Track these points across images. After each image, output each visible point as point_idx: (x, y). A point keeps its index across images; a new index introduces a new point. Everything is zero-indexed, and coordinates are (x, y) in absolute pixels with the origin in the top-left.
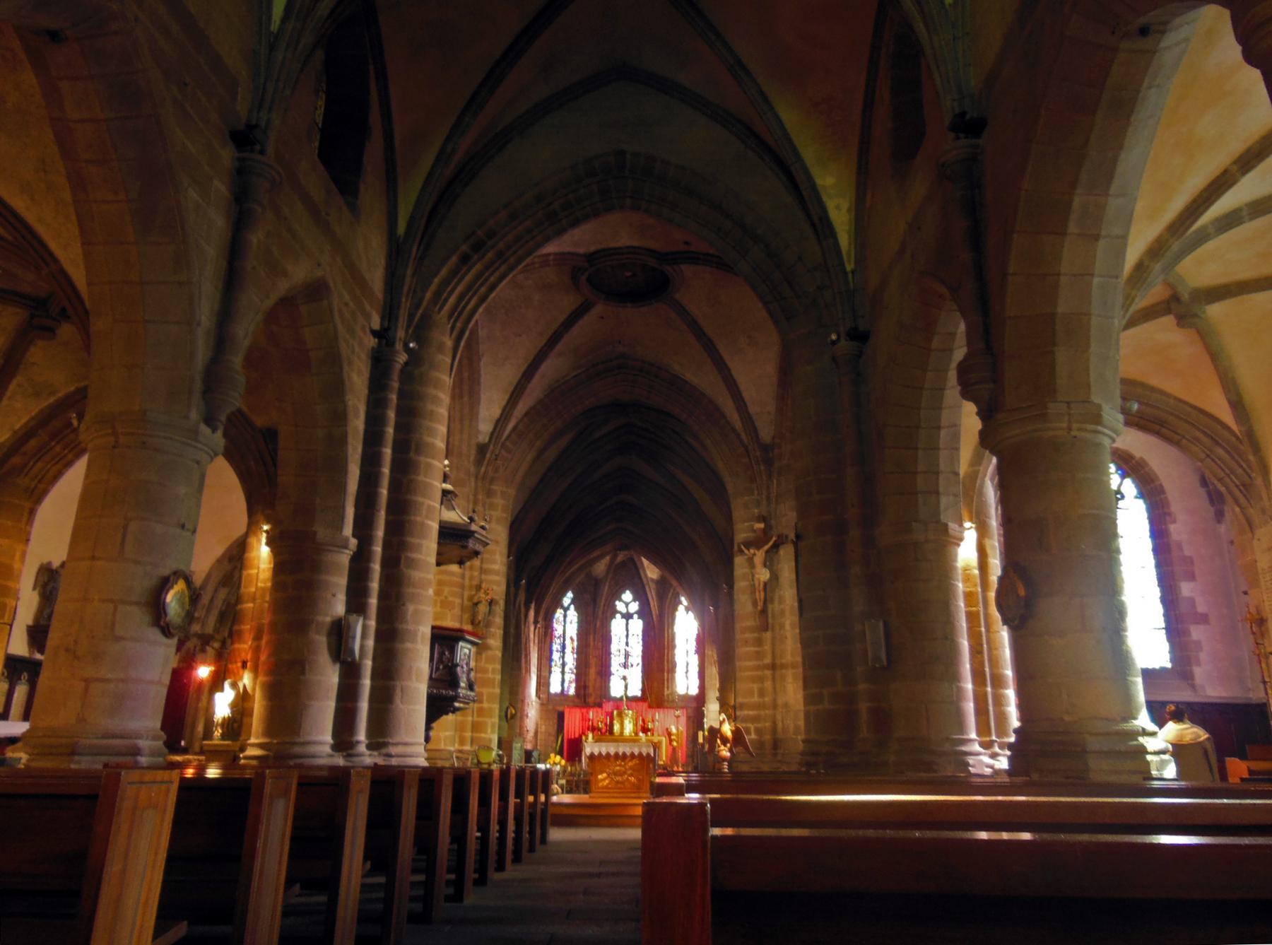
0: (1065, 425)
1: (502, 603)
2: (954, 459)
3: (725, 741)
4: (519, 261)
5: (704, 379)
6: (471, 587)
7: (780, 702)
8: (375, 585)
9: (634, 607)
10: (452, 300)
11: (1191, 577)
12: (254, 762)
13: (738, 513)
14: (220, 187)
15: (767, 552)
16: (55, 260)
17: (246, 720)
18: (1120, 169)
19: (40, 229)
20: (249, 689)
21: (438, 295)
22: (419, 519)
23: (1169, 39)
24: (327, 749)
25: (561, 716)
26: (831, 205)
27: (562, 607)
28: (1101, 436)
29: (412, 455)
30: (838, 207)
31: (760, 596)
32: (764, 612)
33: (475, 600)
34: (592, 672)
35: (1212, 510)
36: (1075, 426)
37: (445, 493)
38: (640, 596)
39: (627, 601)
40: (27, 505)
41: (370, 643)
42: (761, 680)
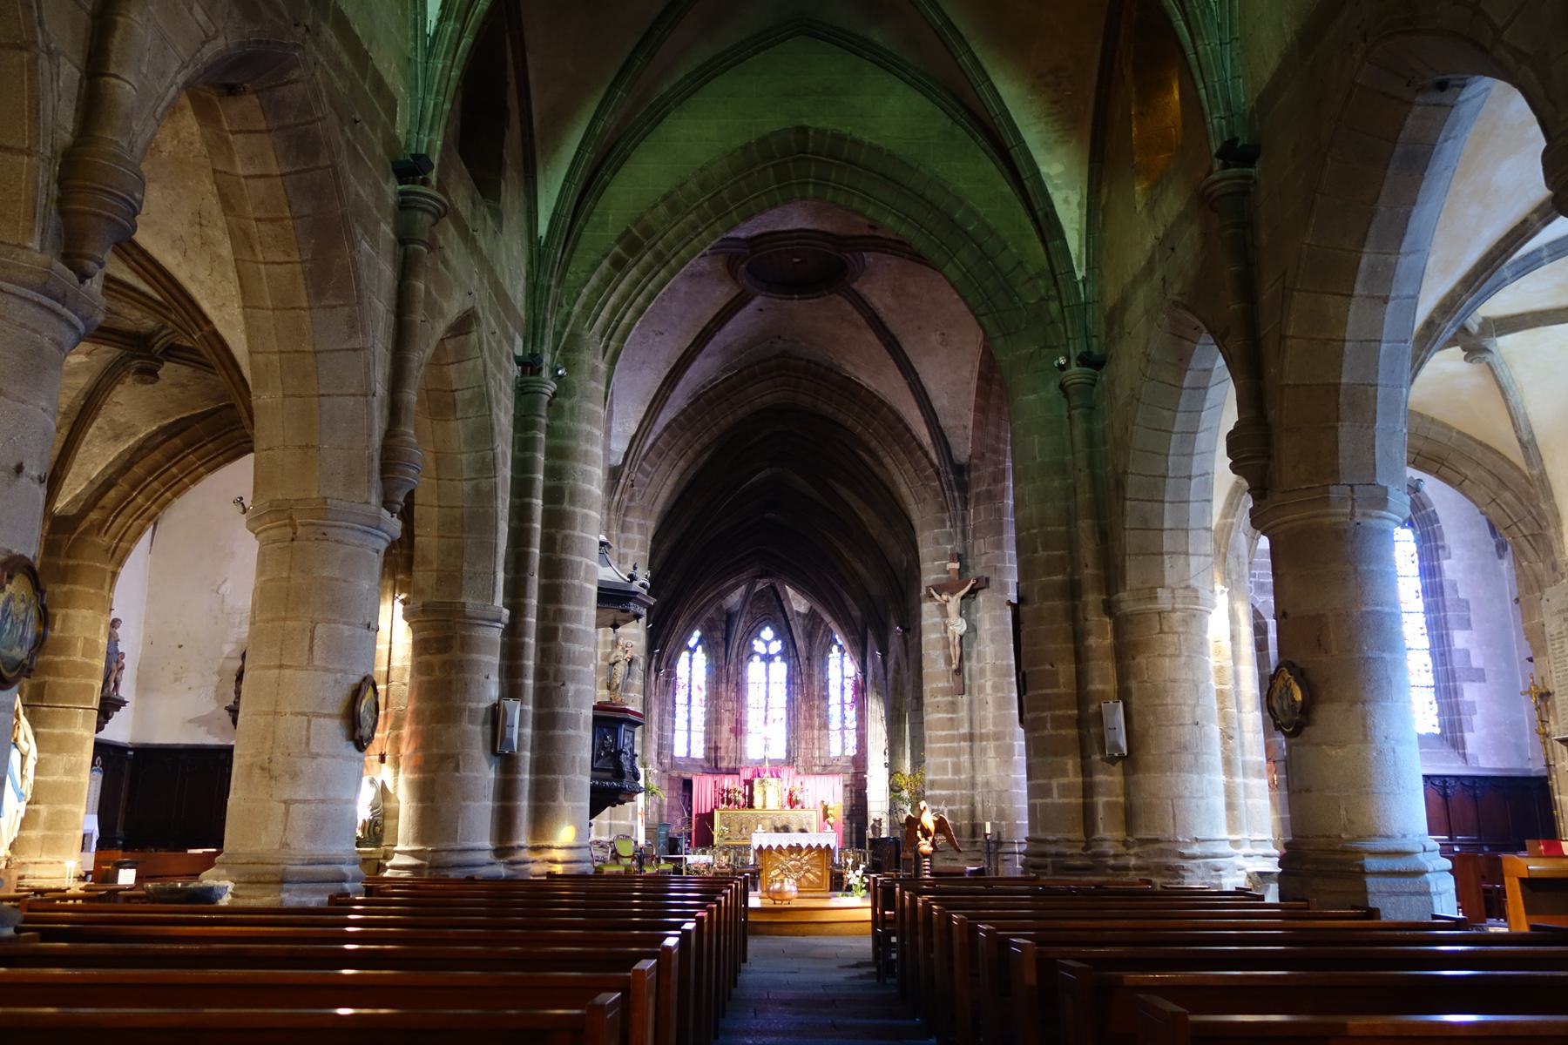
0: (1348, 510)
1: (641, 661)
2: (1206, 513)
3: (926, 833)
4: (682, 264)
5: (890, 387)
6: (605, 642)
7: (979, 779)
8: (530, 663)
9: (776, 647)
10: (604, 314)
11: (1466, 624)
12: (405, 874)
13: (926, 550)
14: (386, 229)
15: (963, 598)
16: (208, 322)
17: (389, 823)
18: (1412, 225)
19: (194, 290)
20: (390, 787)
21: (587, 308)
22: (576, 582)
23: (1467, 93)
24: (488, 856)
25: (688, 785)
26: (1057, 198)
27: (688, 648)
28: (1386, 522)
29: (566, 506)
30: (1066, 201)
31: (955, 652)
32: (959, 671)
33: (612, 660)
34: (725, 728)
35: (1493, 542)
36: (1358, 511)
37: (602, 544)
38: (784, 632)
39: (767, 640)
40: (110, 568)
41: (528, 731)
42: (956, 753)
